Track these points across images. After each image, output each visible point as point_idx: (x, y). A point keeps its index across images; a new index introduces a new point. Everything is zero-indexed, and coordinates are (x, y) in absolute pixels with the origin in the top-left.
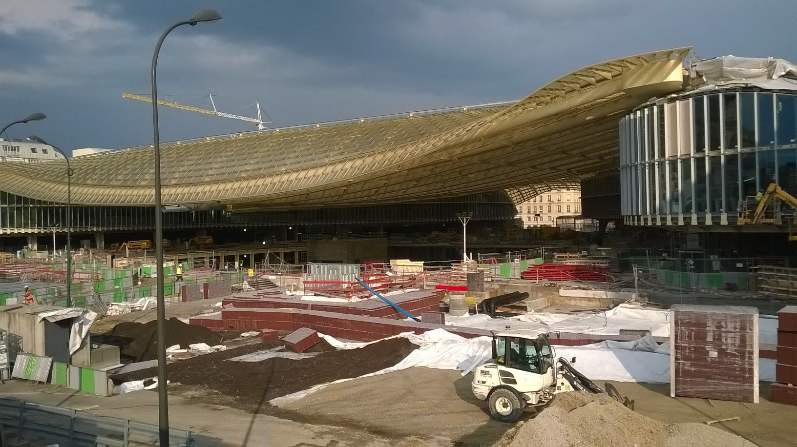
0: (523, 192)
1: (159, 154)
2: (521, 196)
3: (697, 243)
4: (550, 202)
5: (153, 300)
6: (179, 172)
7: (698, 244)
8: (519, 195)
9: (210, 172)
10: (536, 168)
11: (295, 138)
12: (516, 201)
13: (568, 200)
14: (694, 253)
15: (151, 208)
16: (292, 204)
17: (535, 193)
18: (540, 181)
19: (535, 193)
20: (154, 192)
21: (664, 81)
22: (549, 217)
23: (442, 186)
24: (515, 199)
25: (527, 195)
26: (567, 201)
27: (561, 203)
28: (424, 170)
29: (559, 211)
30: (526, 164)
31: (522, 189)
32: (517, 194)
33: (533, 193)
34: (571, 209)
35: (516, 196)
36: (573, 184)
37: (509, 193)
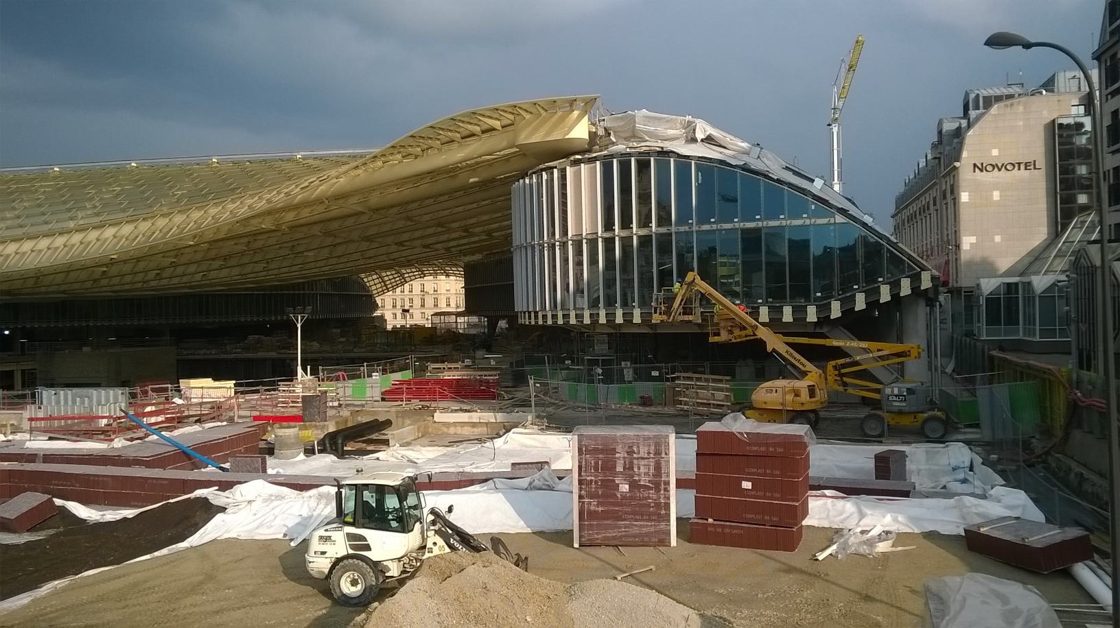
0: (386, 278)
12: (376, 292)
13: (447, 290)
17: (403, 280)
19: (403, 280)
22: (393, 314)
24: (374, 288)
25: (391, 283)
26: (445, 292)
29: (436, 306)
31: (384, 274)
32: (377, 281)
33: (400, 280)
36: (453, 269)
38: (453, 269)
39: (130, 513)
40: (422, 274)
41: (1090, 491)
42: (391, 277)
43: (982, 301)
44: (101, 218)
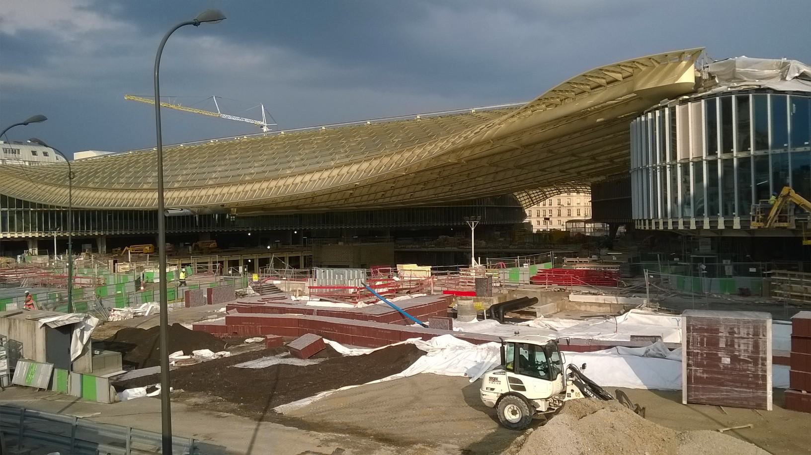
0: (533, 195)
1: (162, 157)
2: (530, 199)
3: (709, 247)
4: (559, 206)
6: (182, 175)
7: (710, 248)
8: (528, 199)
9: (214, 175)
11: (300, 140)
13: (578, 204)
14: (706, 258)
15: (153, 212)
16: (297, 207)
17: (545, 197)
18: (549, 185)
19: (545, 197)
20: (156, 195)
21: (676, 82)
23: (450, 189)
24: (524, 202)
25: (536, 199)
26: (576, 205)
27: (571, 207)
28: (431, 173)
29: (569, 215)
30: (535, 167)
32: (526, 198)
33: (543, 196)
34: (581, 213)
35: (525, 200)
36: (583, 187)
37: (518, 197)
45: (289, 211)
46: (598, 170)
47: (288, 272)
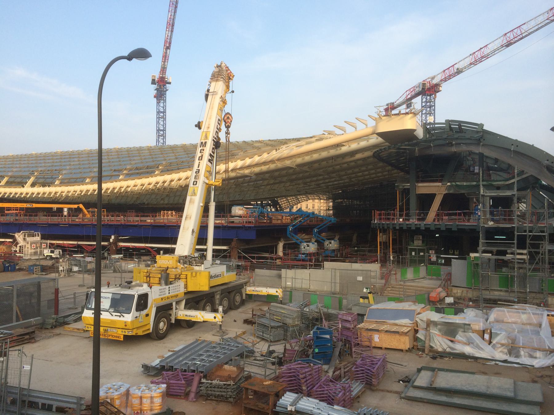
0: (290, 201)
2: (288, 203)
5: (96, 186)
8: (287, 203)
10: (307, 184)
14: (418, 249)
18: (310, 194)
24: (284, 205)
30: (300, 181)
31: (289, 198)
32: (285, 202)
33: (297, 201)
35: (284, 203)
36: (315, 196)
37: (279, 201)
38: (315, 196)
39: (11, 234)
40: (308, 198)
41: (293, 410)
42: (292, 200)
43: (13, 234)
44: (154, 163)
45: (125, 238)
46: (35, 205)
47: (191, 263)
